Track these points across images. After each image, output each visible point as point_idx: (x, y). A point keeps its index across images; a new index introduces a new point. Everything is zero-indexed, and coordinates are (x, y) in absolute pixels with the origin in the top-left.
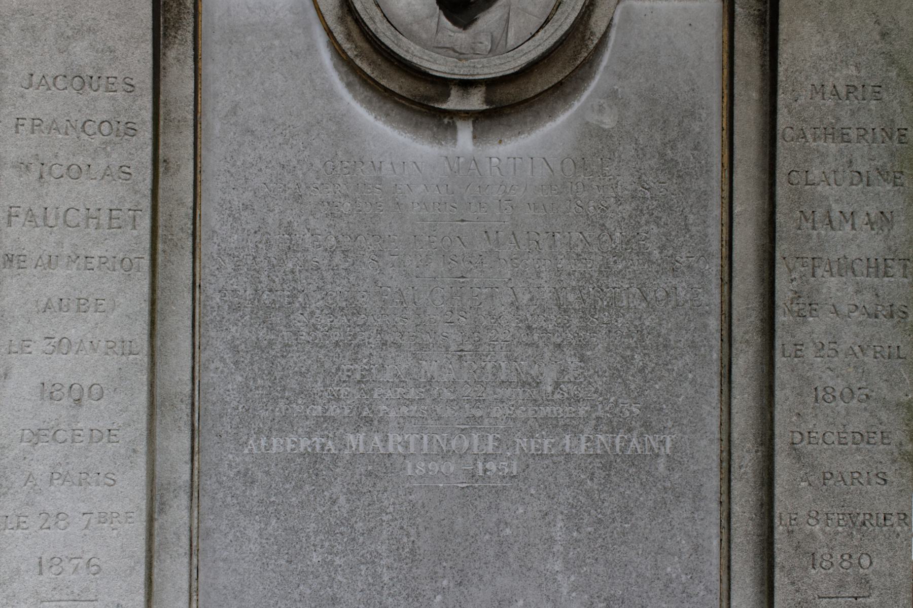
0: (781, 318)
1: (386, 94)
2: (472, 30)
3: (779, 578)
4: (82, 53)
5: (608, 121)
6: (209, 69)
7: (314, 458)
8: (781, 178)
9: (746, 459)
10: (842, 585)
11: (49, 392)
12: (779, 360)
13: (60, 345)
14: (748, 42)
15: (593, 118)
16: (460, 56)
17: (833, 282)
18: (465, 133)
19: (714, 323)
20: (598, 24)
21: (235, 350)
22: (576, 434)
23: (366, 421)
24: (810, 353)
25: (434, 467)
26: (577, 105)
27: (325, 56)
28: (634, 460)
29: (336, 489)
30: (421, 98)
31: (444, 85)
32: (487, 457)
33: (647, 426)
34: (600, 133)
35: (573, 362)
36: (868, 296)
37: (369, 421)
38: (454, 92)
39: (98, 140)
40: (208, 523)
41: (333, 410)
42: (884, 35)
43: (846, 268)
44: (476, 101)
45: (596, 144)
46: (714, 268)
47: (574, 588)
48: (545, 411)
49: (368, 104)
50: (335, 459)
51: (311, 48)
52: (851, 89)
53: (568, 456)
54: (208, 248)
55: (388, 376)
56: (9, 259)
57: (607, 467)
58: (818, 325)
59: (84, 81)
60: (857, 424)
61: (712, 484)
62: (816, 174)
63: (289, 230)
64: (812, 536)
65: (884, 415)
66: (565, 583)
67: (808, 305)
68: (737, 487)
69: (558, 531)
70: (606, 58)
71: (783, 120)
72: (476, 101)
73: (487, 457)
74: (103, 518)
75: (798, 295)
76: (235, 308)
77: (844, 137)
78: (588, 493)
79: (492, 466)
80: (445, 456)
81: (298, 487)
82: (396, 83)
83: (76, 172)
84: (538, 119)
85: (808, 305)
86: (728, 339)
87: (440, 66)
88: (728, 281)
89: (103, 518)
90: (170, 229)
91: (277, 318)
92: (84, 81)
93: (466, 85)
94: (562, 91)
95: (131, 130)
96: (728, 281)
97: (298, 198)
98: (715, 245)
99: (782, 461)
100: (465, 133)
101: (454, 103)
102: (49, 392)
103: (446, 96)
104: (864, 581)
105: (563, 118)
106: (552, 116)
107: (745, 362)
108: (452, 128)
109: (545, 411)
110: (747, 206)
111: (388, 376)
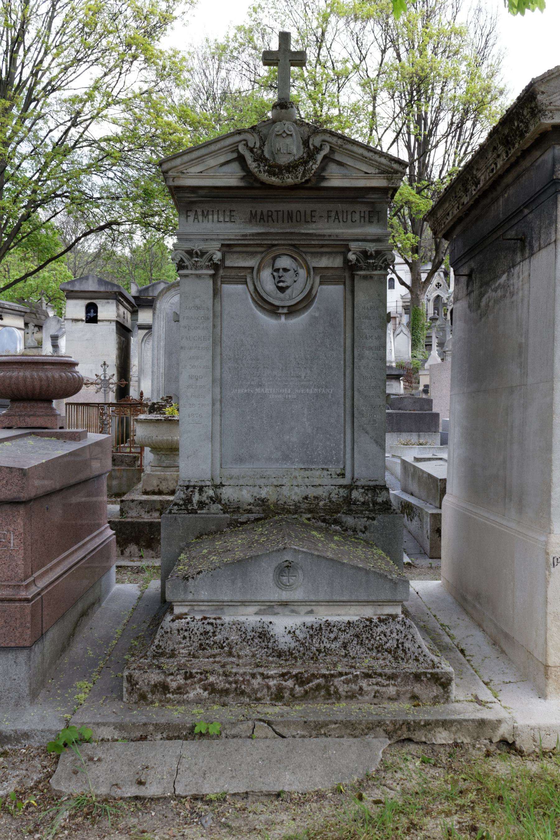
0: (355, 360)
1: (264, 309)
2: (278, 33)
3: (355, 420)
4: (197, 302)
5: (317, 315)
6: (223, 303)
7: (248, 394)
8: (355, 328)
9: (349, 394)
10: (370, 421)
11: (191, 377)
12: (355, 370)
13: (193, 367)
14: (349, 296)
15: (313, 314)
16: (282, 300)
17: (367, 352)
18: (283, 318)
19: (342, 362)
20: (314, 292)
21: (229, 369)
22: (310, 388)
23: (260, 385)
24: (362, 368)
25: (276, 396)
26: (309, 311)
27: (250, 300)
28: (323, 395)
29: (253, 401)
30: (273, 310)
31: (278, 307)
32: (288, 394)
33: (327, 387)
34: (315, 318)
35: (309, 372)
36: (375, 355)
37: (261, 386)
38: (280, 309)
39: (201, 321)
40: (224, 409)
41: (252, 383)
42: (379, 295)
43: (370, 348)
44: (285, 311)
45: (314, 320)
46: (342, 349)
47: (309, 425)
48: (302, 383)
49: (260, 311)
50: (253, 394)
51: (247, 298)
52: (371, 308)
53: (308, 394)
54: (224, 345)
55: (265, 375)
56: (182, 348)
57: (317, 396)
58: (364, 362)
59: (198, 308)
60: (373, 384)
61: (342, 401)
62: (363, 327)
63: (242, 341)
64: (363, 410)
65: (379, 383)
66: (307, 424)
67: (361, 357)
68: (347, 400)
69: (306, 411)
70: (316, 300)
71: (356, 315)
72: (285, 311)
73: (288, 394)
74: (203, 405)
75: (359, 355)
76: (229, 359)
77: (369, 319)
78: (313, 403)
79: (290, 396)
80: (279, 394)
81: (245, 401)
82: (267, 307)
83: (196, 328)
84: (300, 315)
85: (361, 357)
86: (345, 366)
87: (277, 303)
88: (345, 353)
89: (203, 405)
90: (217, 341)
91: (239, 361)
92: (198, 308)
93: (283, 307)
94: (306, 307)
95: (208, 319)
96: (345, 353)
97: (244, 333)
98: (342, 344)
99: (356, 393)
100: (283, 318)
101: (280, 311)
102: (191, 377)
103: (278, 309)
104: (374, 421)
105: (306, 314)
106: (303, 313)
107: (348, 371)
108: (280, 317)
109: (302, 383)
110: (349, 334)
111: (265, 375)
